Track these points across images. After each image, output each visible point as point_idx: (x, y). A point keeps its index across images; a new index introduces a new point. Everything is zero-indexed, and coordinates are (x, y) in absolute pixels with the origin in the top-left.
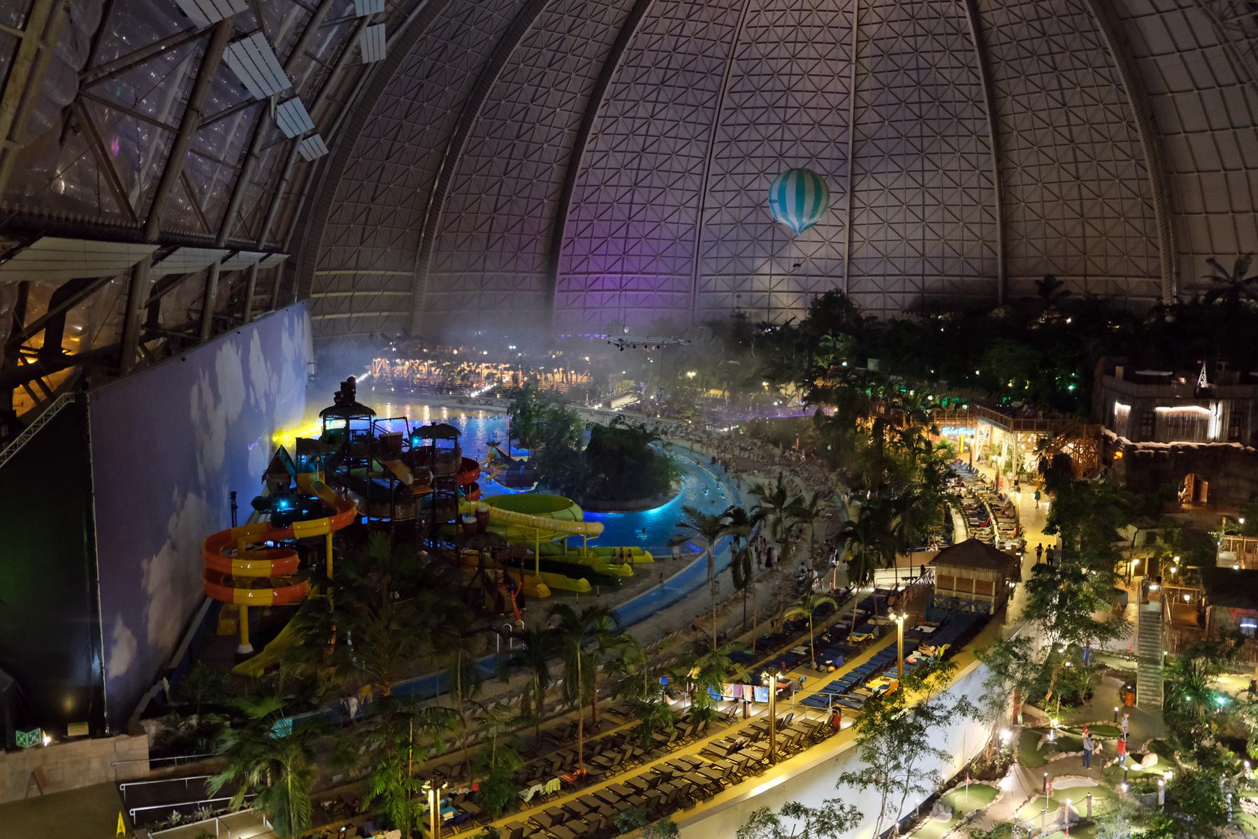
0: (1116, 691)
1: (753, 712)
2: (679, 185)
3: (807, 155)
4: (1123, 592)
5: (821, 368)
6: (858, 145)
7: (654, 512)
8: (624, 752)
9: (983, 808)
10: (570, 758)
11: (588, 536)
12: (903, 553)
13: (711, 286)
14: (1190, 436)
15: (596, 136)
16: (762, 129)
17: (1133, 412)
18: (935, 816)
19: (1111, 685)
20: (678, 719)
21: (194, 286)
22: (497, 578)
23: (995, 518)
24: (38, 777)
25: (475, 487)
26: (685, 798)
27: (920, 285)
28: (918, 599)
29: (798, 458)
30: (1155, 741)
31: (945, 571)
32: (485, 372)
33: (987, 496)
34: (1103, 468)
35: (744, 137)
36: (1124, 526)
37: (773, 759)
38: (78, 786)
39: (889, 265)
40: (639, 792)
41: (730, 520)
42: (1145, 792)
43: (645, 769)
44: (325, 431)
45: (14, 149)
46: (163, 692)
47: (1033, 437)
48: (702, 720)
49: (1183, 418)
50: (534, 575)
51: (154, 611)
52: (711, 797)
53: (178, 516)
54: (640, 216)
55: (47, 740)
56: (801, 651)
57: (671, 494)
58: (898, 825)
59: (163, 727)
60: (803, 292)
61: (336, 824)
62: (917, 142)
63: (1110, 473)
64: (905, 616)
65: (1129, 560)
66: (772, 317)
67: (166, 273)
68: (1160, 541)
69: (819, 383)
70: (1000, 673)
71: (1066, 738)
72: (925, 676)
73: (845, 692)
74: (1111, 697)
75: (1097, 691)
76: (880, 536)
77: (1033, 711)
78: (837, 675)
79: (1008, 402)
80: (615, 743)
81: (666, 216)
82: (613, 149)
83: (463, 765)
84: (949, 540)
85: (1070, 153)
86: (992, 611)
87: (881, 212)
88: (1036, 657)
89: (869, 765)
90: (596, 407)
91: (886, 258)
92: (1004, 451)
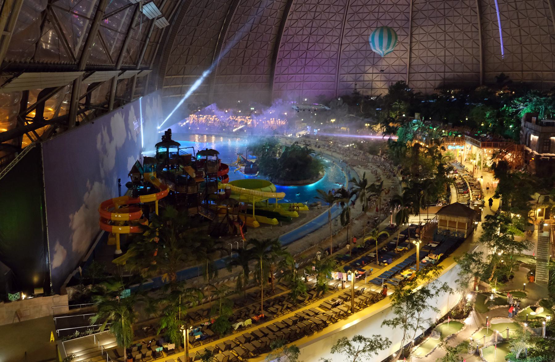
0: (526, 275)
1: (347, 286)
2: (330, 34)
3: (390, 18)
4: (532, 225)
5: (392, 118)
6: (414, 13)
7: (311, 186)
8: (283, 305)
9: (456, 333)
10: (258, 308)
11: (278, 198)
12: (424, 208)
13: (345, 79)
15: (292, 13)
16: (369, 7)
17: (539, 139)
18: (432, 336)
19: (524, 272)
20: (310, 288)
21: (107, 85)
22: (234, 219)
23: (471, 189)
24: (18, 314)
25: (226, 176)
26: (308, 331)
27: (443, 77)
28: (429, 231)
29: (380, 159)
30: (543, 300)
31: (443, 218)
32: (240, 120)
33: (468, 179)
34: (525, 165)
35: (361, 11)
36: (533, 194)
37: (353, 310)
38: (36, 318)
39: (428, 68)
40: (288, 326)
41: (340, 194)
42: (537, 326)
43: (291, 314)
44: (157, 153)
45: (10, 35)
46: (79, 273)
47: (490, 151)
48: (322, 290)
50: (252, 217)
51: (76, 237)
52: (321, 329)
53: (89, 193)
54: (313, 48)
55: (24, 296)
56: (372, 255)
57: (320, 177)
58: (413, 341)
59: (76, 290)
60: (388, 81)
61: (146, 339)
62: (442, 11)
63: (528, 168)
64: (420, 242)
65: (535, 209)
66: (373, 92)
67: (92, 82)
68: (551, 201)
69: (391, 125)
70: (465, 269)
71: (499, 298)
72: (427, 272)
73: (391, 277)
74: (523, 279)
75: (516, 274)
76: (414, 200)
77: (484, 284)
78: (388, 268)
79: (481, 133)
80: (280, 301)
81: (324, 48)
82: (300, 18)
83: (209, 310)
84: (448, 201)
85: (516, 14)
86: (465, 236)
87: (425, 44)
88: (485, 260)
89: (398, 316)
90: (289, 136)
91: (427, 65)
92: (478, 156)
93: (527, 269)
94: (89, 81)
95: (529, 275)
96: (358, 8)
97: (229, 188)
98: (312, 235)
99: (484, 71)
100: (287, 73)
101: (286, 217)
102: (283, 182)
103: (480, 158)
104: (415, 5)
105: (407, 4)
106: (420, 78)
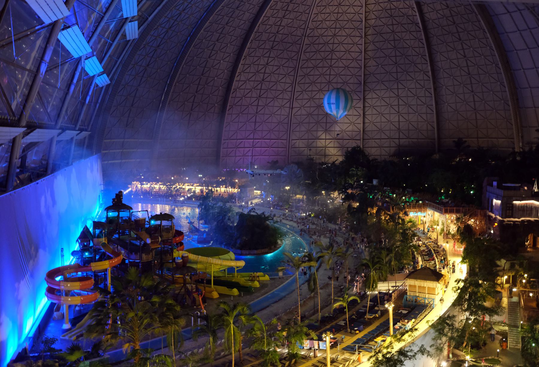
1: (319, 354)
2: (280, 96)
4: (500, 292)
5: (351, 184)
7: (269, 255)
11: (237, 268)
14: (530, 216)
23: (436, 256)
25: (182, 244)
35: (312, 73)
47: (454, 216)
49: (527, 206)
50: (211, 287)
56: (342, 323)
57: (278, 246)
60: (341, 147)
64: (393, 305)
65: (502, 276)
66: (327, 159)
68: (517, 267)
69: (350, 191)
70: (440, 333)
71: (474, 365)
77: (457, 352)
78: (360, 335)
91: (381, 130)
92: (440, 223)
93: (499, 336)
94: (30, 138)
95: (501, 341)
96: (309, 70)
97: (186, 255)
98: (276, 306)
99: (439, 138)
100: (235, 138)
101: (247, 287)
102: (239, 252)
103: (443, 224)
104: (367, 68)
105: (359, 67)
106: (374, 144)
